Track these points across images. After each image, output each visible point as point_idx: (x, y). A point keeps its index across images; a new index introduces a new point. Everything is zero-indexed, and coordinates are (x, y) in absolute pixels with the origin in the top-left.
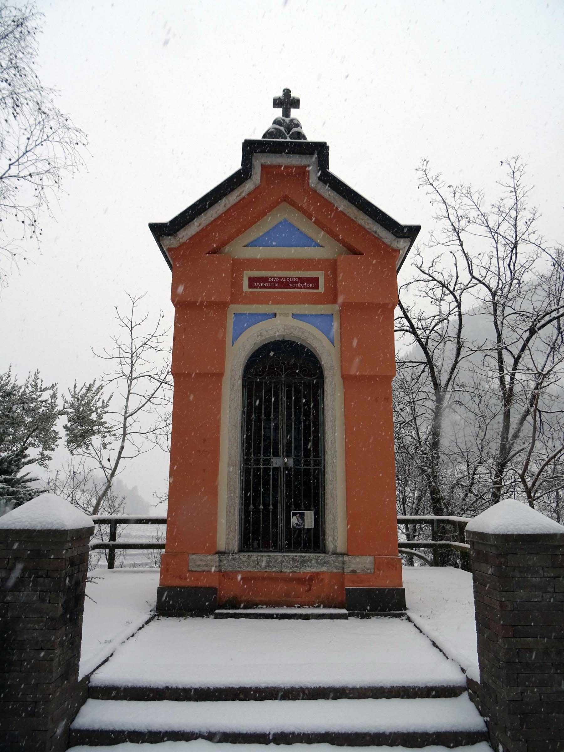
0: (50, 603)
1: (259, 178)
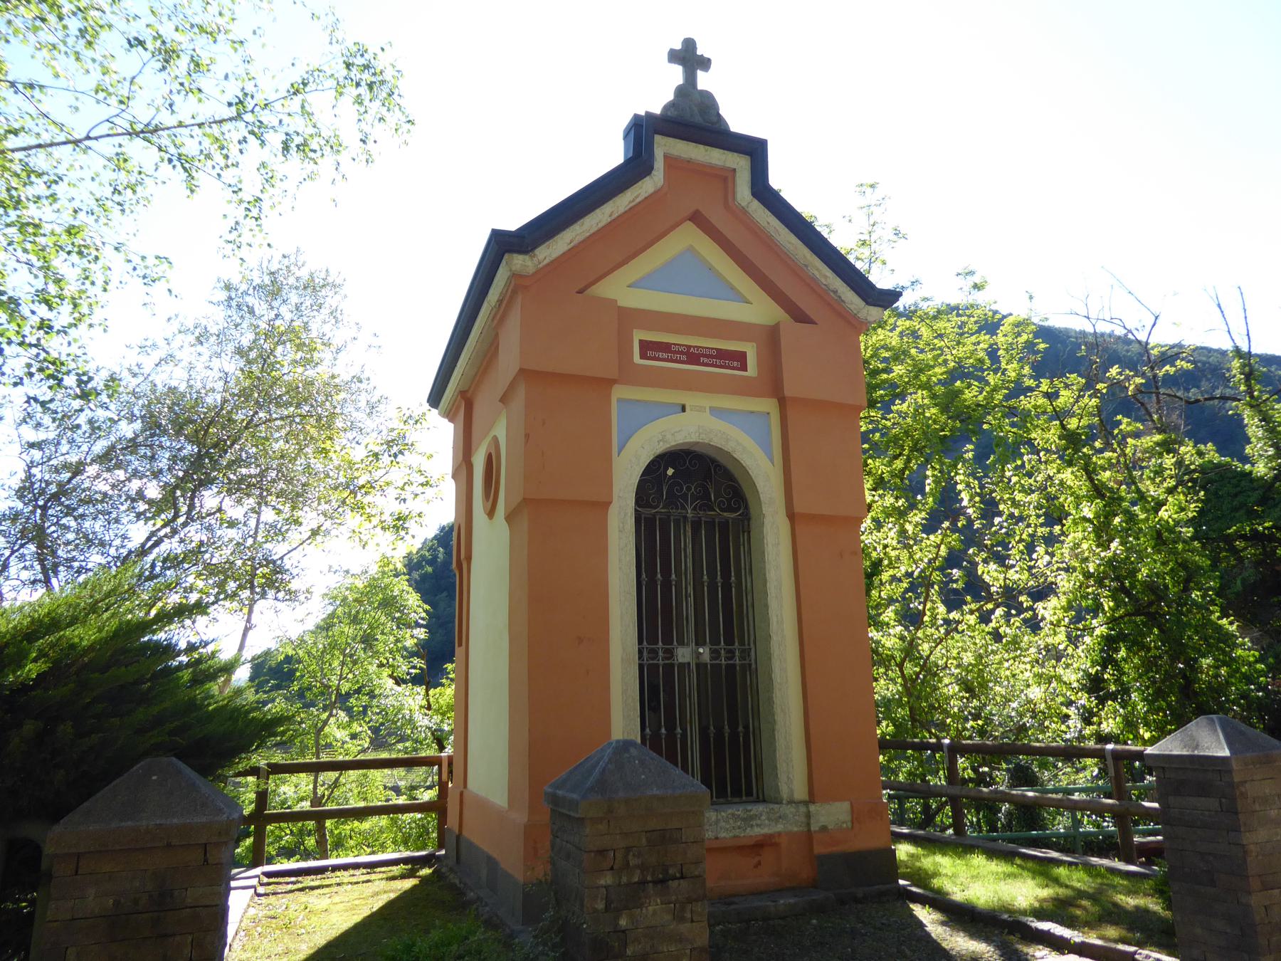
0: (692, 921)
1: (662, 176)
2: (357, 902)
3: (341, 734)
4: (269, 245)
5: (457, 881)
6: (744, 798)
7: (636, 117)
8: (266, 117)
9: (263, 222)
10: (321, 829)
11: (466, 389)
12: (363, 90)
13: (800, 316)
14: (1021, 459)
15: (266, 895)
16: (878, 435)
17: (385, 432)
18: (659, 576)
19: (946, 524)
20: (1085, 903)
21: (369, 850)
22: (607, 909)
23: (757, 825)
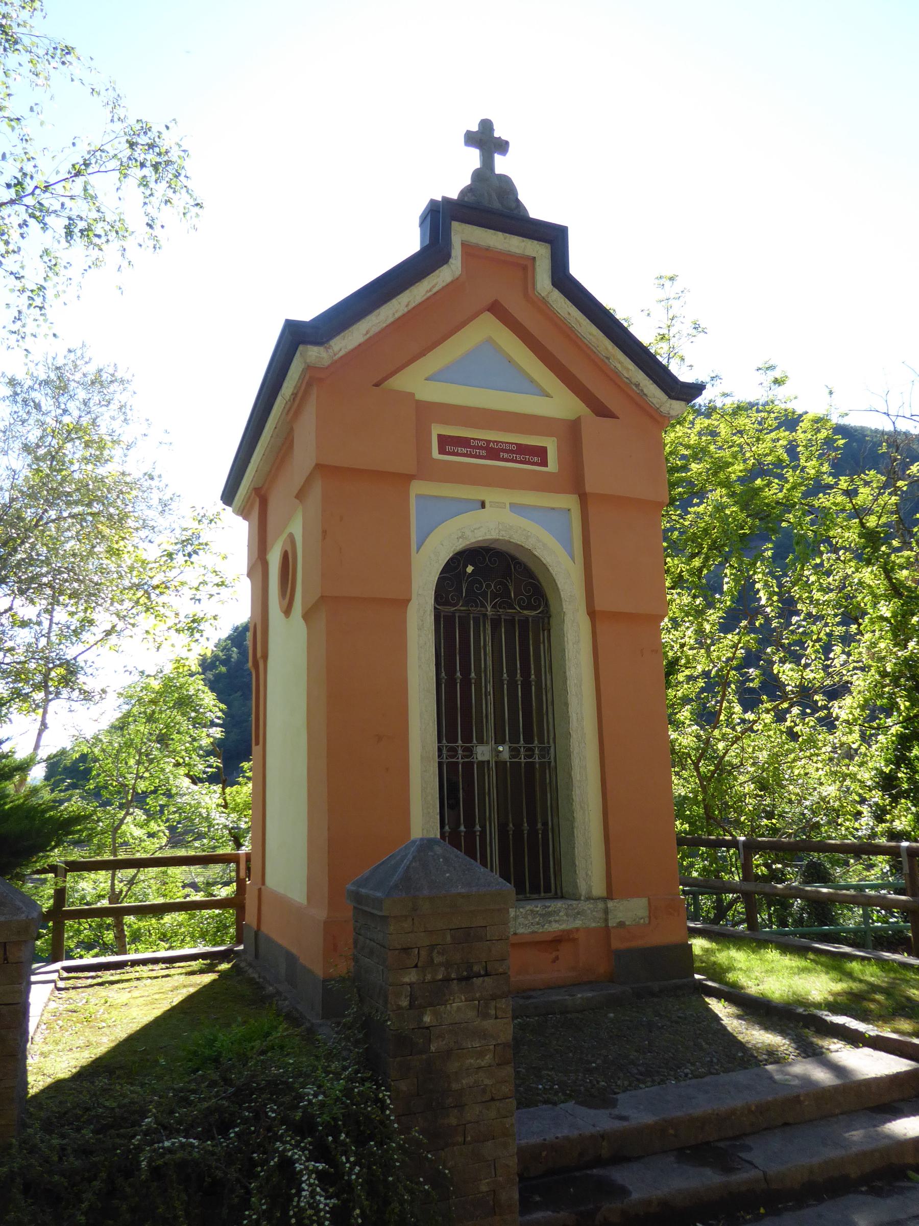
0: (496, 1018)
2: (157, 996)
3: (139, 832)
4: (55, 335)
5: (256, 976)
6: (542, 894)
7: (433, 203)
8: (48, 201)
9: (48, 311)
10: (119, 925)
11: (260, 485)
12: (148, 171)
13: (601, 411)
14: (821, 557)
15: (67, 989)
16: (676, 533)
17: (178, 531)
18: (458, 674)
19: (744, 623)
20: (879, 997)
21: (167, 946)
22: (411, 1006)
23: (556, 921)
